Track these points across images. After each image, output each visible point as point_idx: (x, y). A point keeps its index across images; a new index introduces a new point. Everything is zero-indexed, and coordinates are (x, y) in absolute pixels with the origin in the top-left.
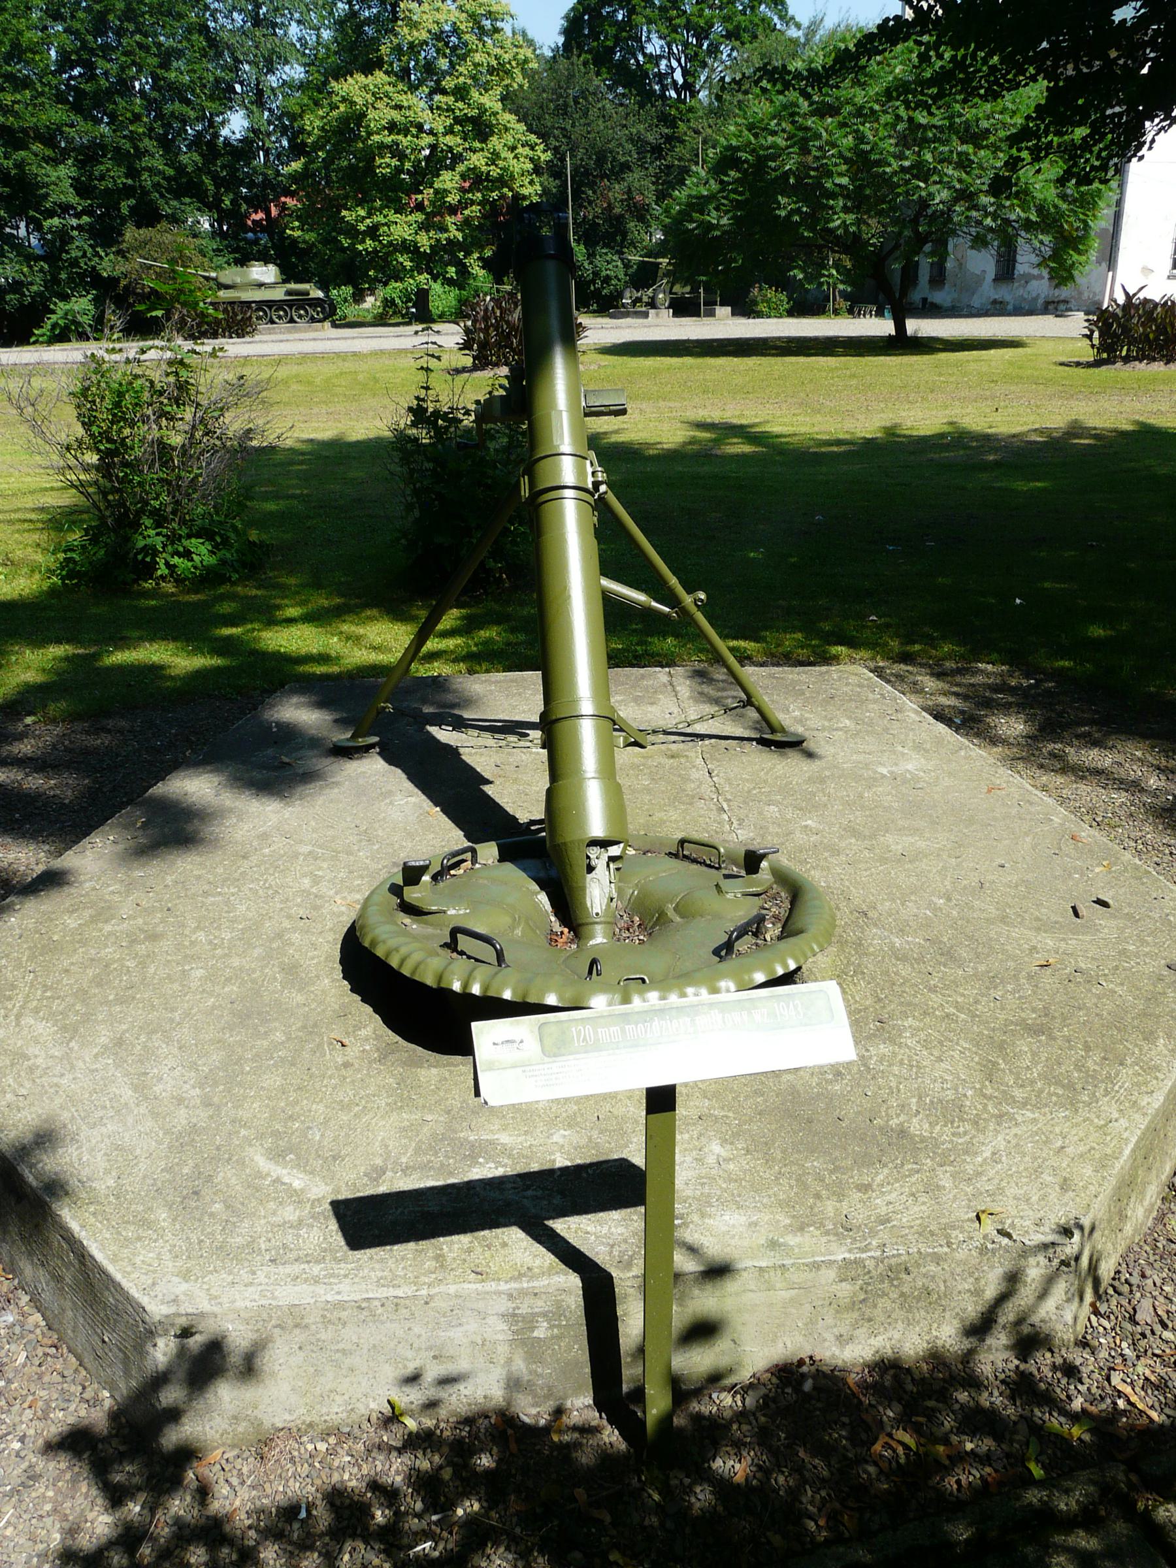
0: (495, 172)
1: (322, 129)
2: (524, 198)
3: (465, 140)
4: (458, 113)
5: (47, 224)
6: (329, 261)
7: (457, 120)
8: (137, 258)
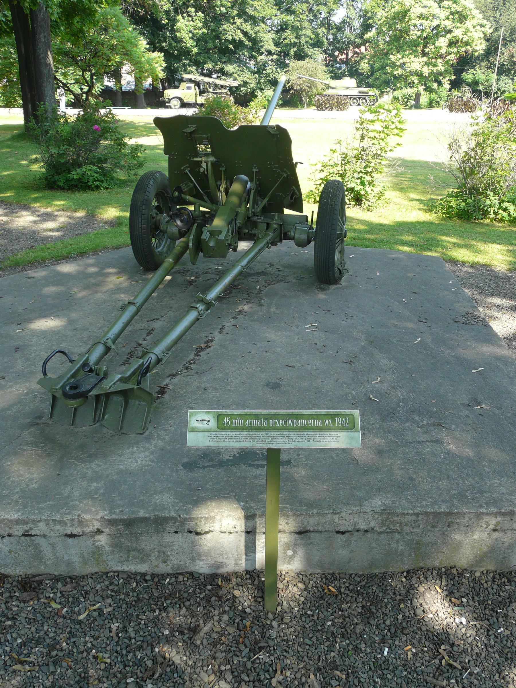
1: (387, 18)
2: (476, 51)
3: (453, 22)
4: (453, 10)
5: (259, 58)
6: (378, 78)
7: (452, 14)
8: (296, 73)
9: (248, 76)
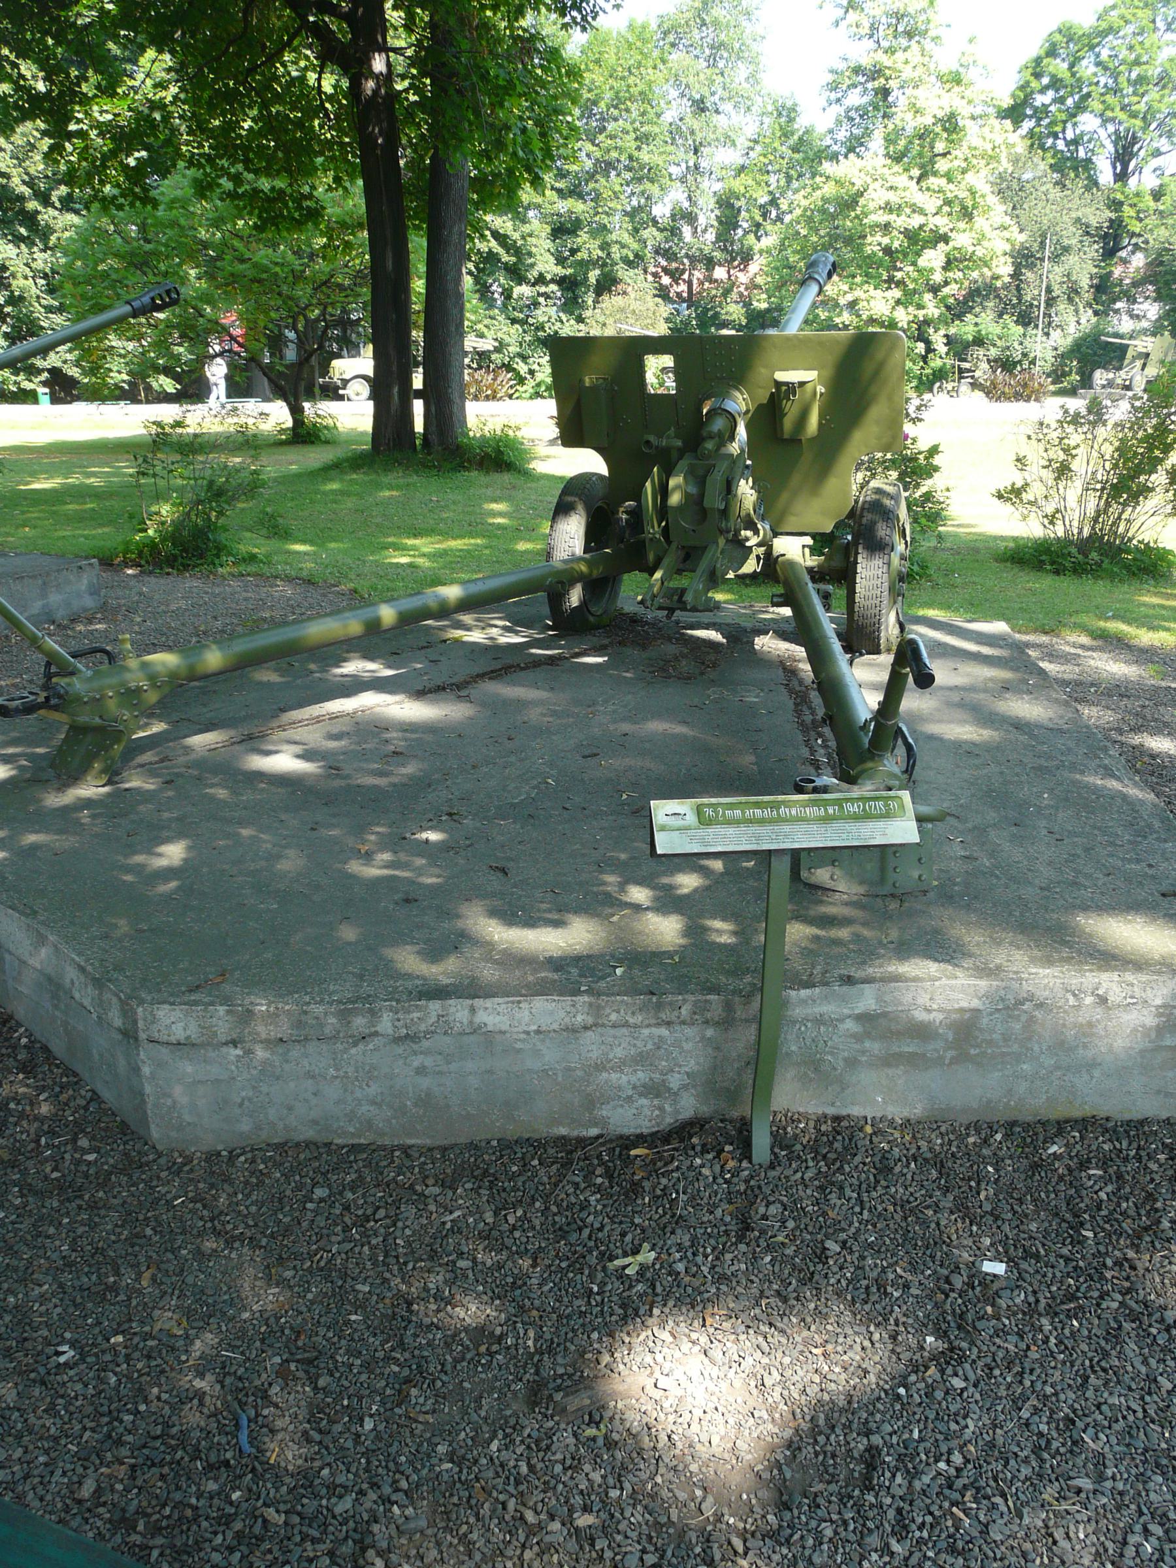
0: (980, 252)
2: (997, 278)
4: (949, 195)
7: (948, 202)
9: (505, 329)
